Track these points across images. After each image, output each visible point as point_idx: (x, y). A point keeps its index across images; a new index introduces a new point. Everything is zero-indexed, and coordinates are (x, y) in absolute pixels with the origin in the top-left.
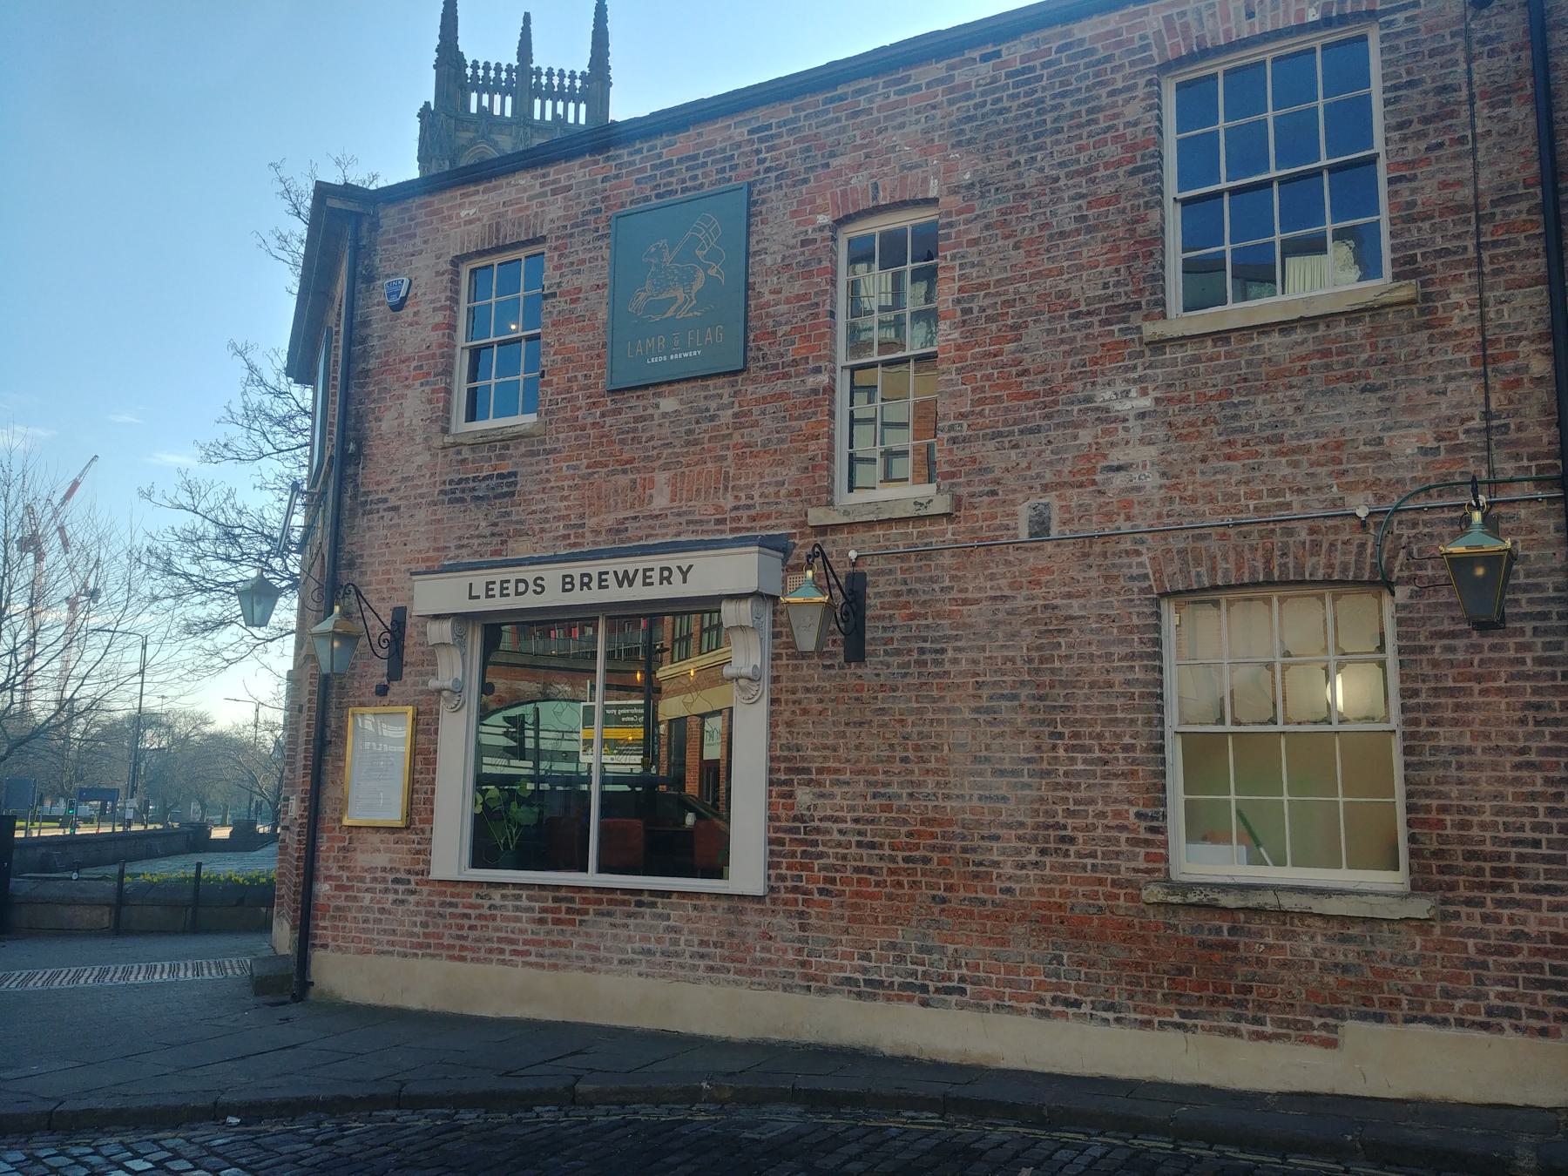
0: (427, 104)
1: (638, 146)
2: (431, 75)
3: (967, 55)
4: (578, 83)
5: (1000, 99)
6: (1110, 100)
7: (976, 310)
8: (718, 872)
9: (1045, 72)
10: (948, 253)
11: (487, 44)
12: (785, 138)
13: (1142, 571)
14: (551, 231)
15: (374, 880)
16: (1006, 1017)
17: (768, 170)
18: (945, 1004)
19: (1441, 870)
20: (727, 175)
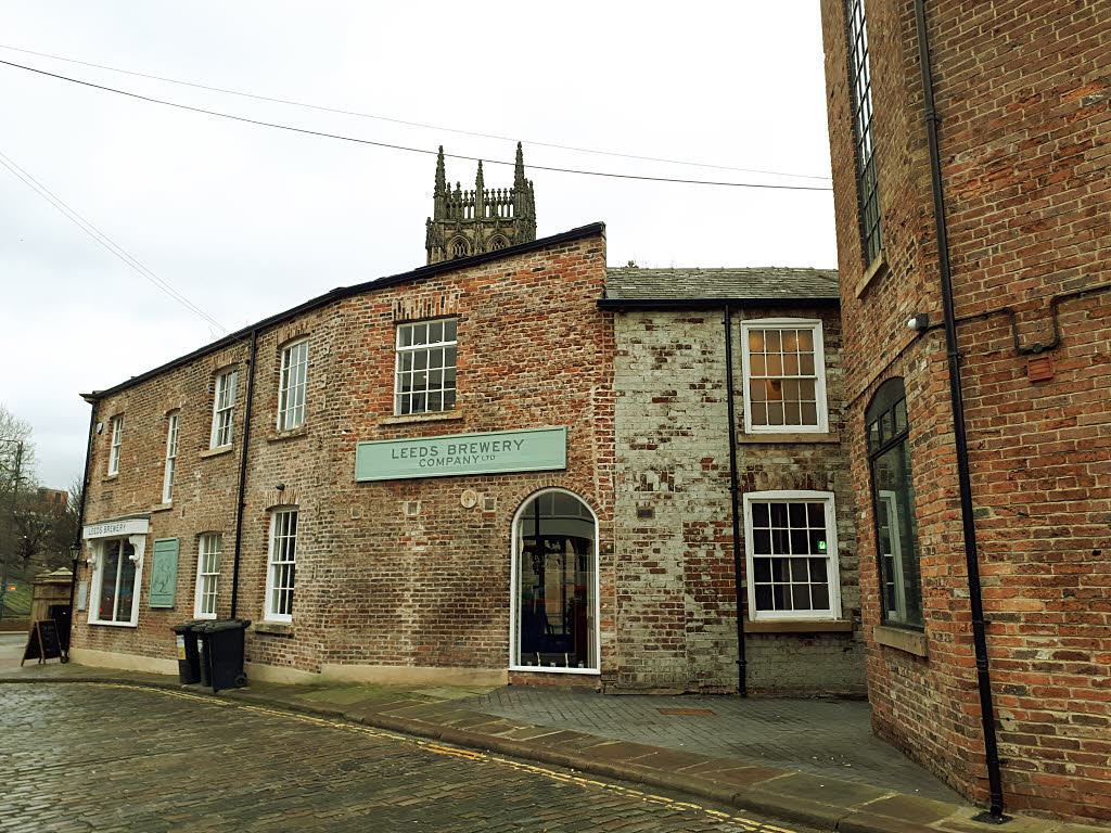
0: (429, 218)
2: (431, 202)
4: (508, 195)
11: (461, 177)
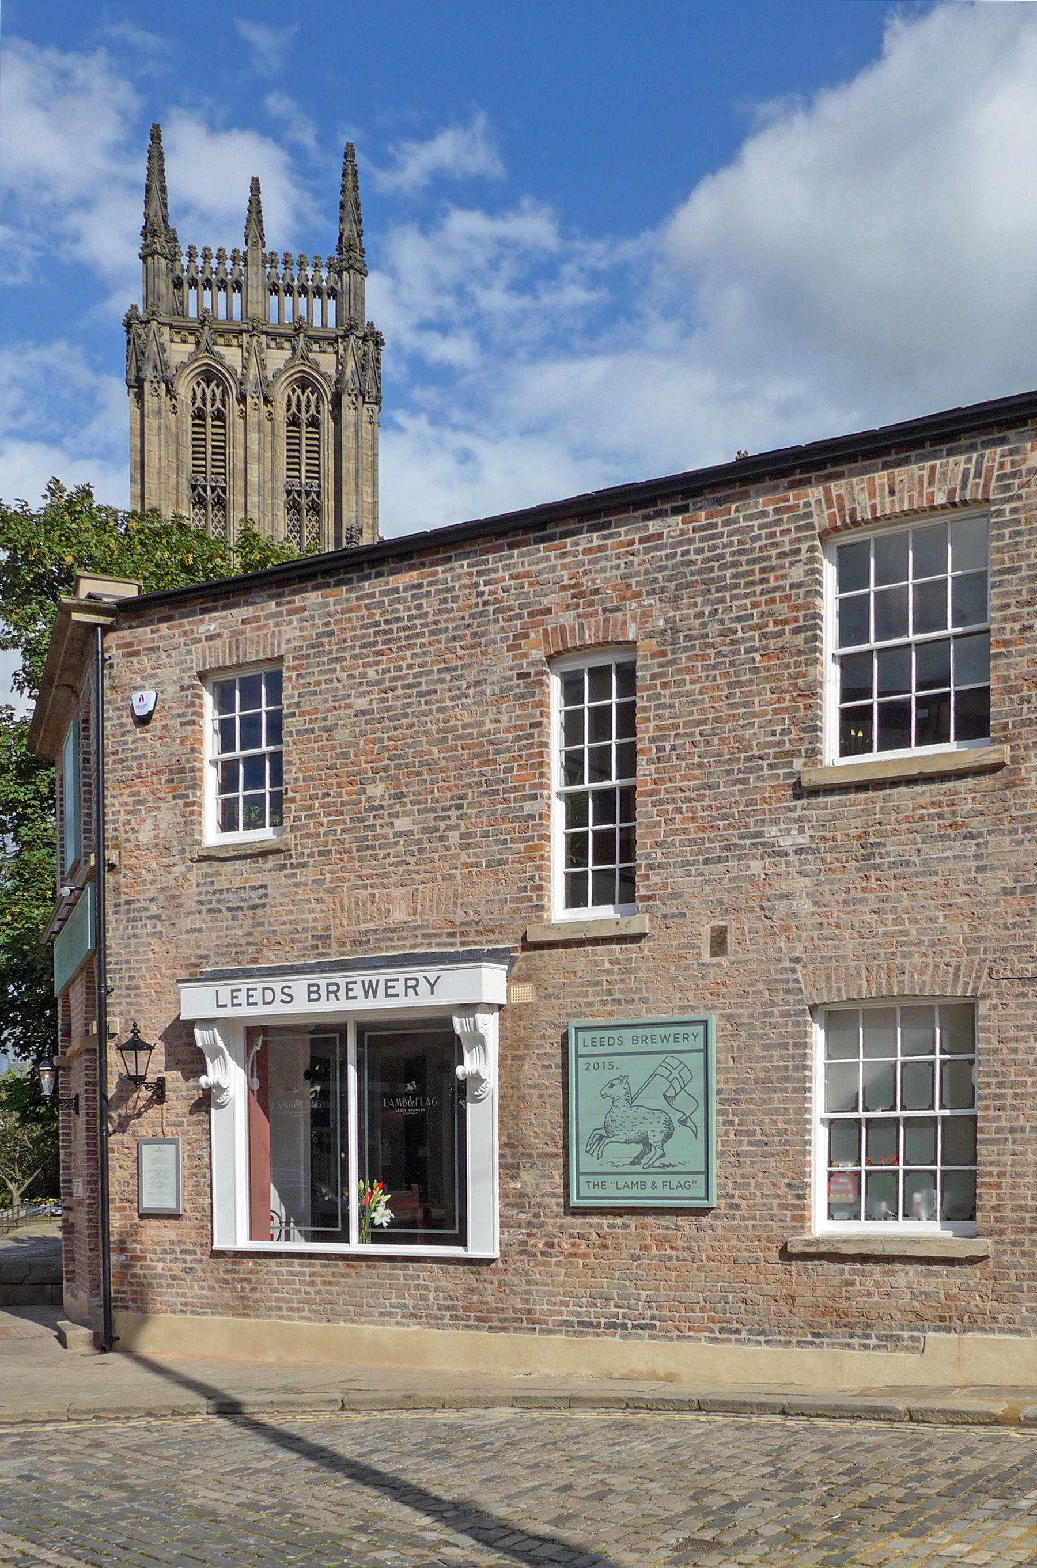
1: (367, 571)
3: (661, 506)
5: (688, 552)
6: (779, 562)
7: (668, 748)
8: (461, 1240)
9: (726, 529)
10: (645, 694)
12: (501, 574)
13: (797, 986)
14: (287, 651)
15: (164, 1251)
16: (686, 1343)
17: (485, 604)
18: (640, 1337)
19: (997, 1220)
20: (449, 606)
